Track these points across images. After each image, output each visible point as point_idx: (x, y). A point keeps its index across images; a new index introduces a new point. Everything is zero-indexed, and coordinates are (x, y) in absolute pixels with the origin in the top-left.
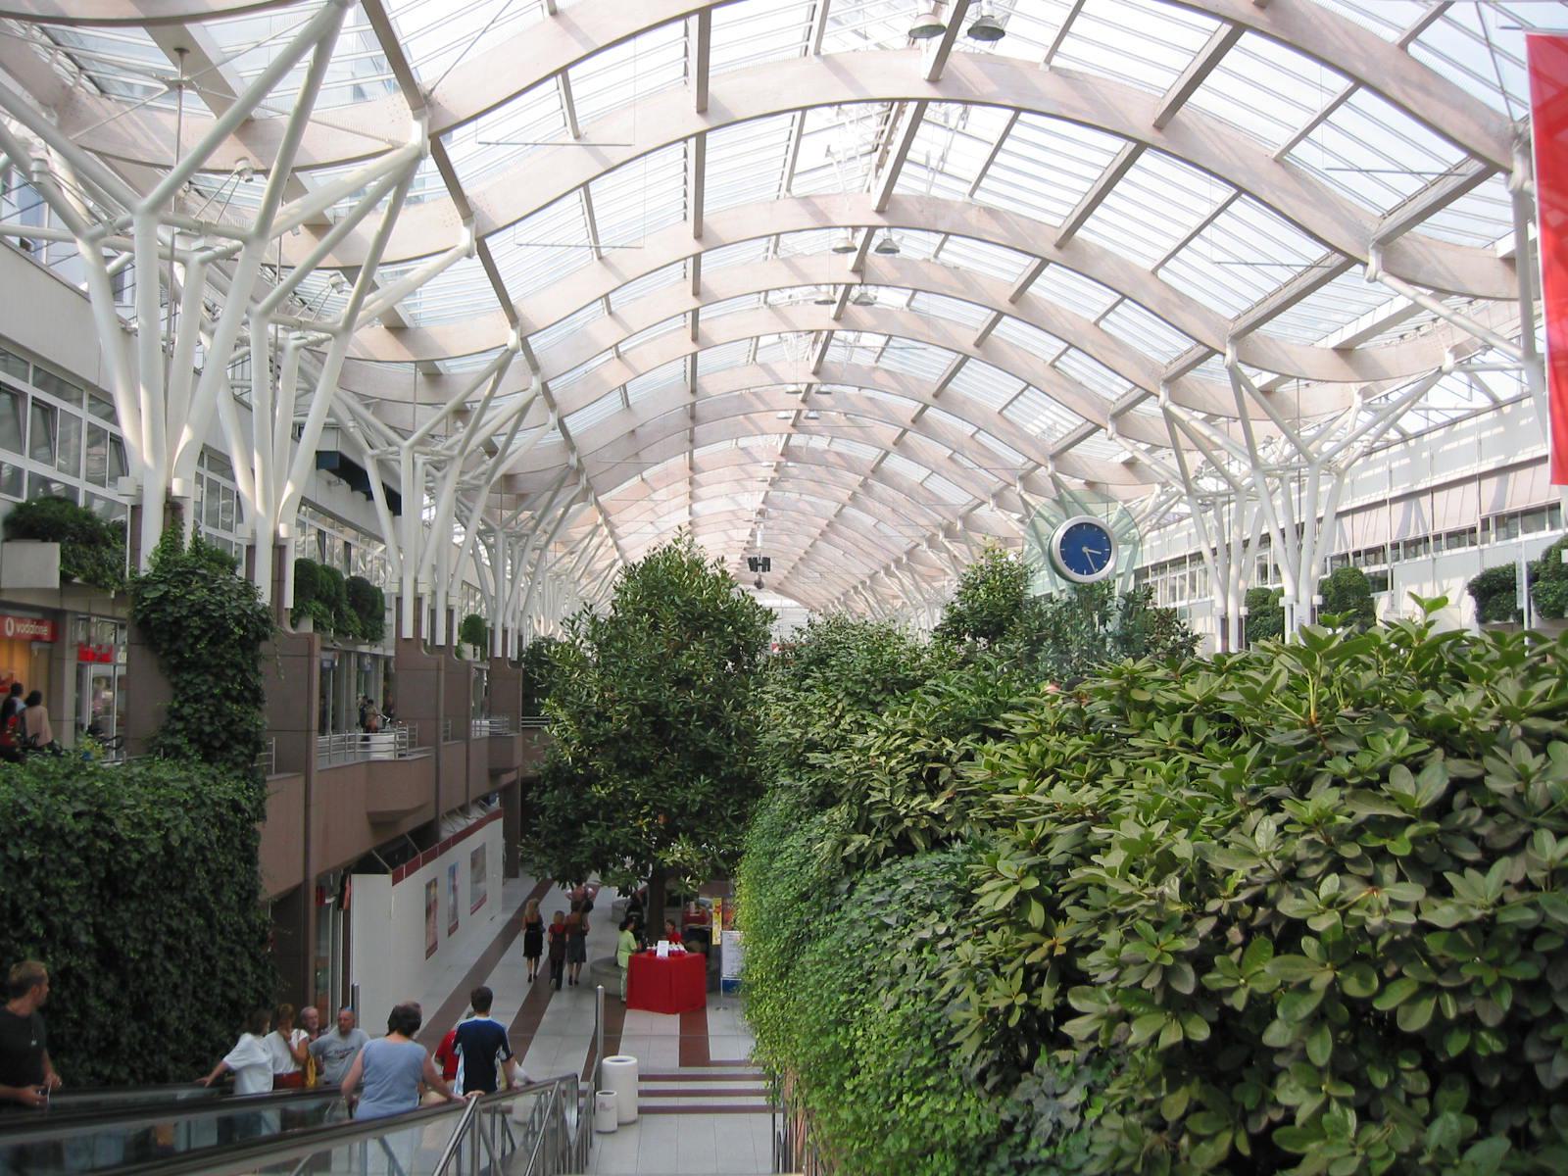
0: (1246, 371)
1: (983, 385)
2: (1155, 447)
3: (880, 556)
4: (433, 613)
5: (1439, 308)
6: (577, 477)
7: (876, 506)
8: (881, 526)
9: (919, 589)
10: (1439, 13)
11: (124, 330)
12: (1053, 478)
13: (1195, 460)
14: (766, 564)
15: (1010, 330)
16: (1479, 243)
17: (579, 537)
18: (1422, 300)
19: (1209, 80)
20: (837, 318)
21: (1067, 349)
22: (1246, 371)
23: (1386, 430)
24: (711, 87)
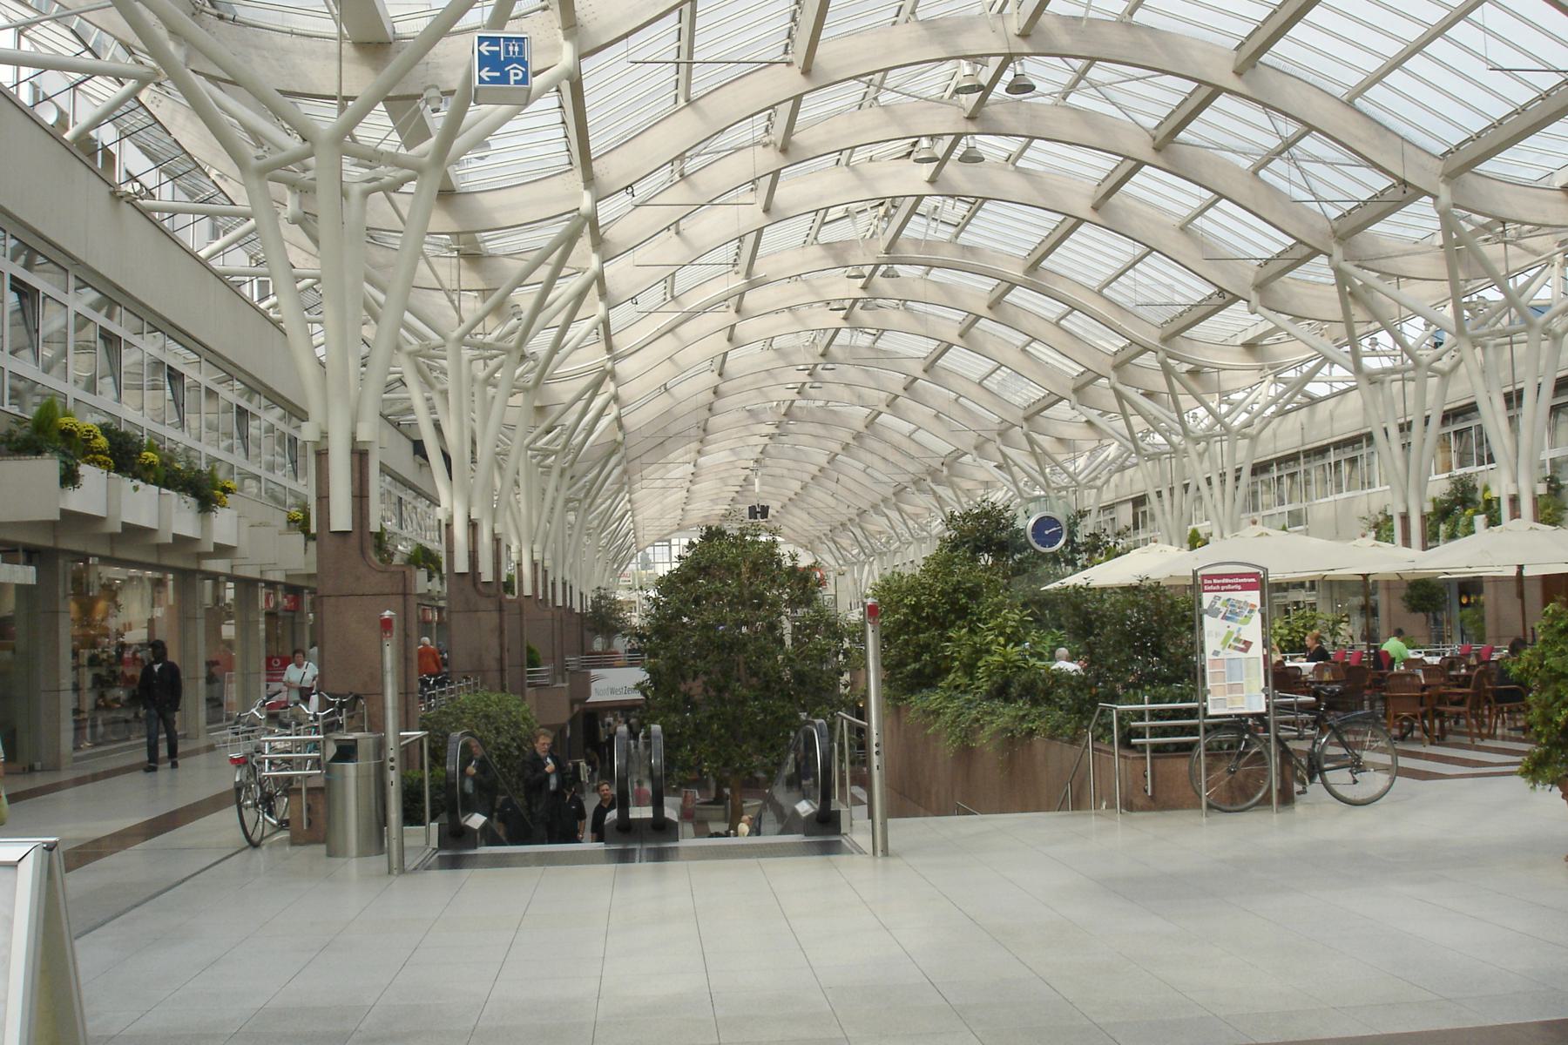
0: (1034, 435)
1: (1090, 256)
2: (1105, 413)
3: (912, 467)
4: (553, 584)
5: (1292, 328)
6: (624, 456)
7: (868, 457)
8: (1037, 349)
9: (905, 523)
10: (1462, 15)
11: (113, 194)
12: (1027, 436)
13: (1136, 421)
14: (764, 511)
15: (1019, 296)
16: (1421, 234)
17: (567, 398)
18: (1282, 325)
19: (1204, 115)
20: (932, 181)
21: (1217, 201)
22: (1034, 435)
23: (1295, 395)
24: (819, 51)
